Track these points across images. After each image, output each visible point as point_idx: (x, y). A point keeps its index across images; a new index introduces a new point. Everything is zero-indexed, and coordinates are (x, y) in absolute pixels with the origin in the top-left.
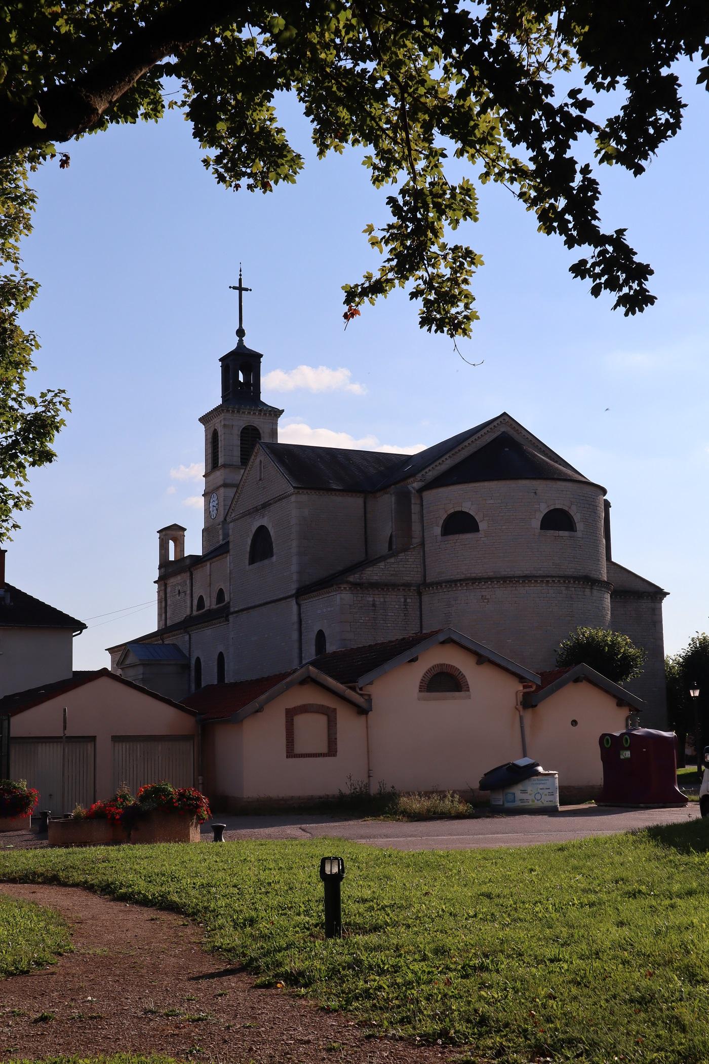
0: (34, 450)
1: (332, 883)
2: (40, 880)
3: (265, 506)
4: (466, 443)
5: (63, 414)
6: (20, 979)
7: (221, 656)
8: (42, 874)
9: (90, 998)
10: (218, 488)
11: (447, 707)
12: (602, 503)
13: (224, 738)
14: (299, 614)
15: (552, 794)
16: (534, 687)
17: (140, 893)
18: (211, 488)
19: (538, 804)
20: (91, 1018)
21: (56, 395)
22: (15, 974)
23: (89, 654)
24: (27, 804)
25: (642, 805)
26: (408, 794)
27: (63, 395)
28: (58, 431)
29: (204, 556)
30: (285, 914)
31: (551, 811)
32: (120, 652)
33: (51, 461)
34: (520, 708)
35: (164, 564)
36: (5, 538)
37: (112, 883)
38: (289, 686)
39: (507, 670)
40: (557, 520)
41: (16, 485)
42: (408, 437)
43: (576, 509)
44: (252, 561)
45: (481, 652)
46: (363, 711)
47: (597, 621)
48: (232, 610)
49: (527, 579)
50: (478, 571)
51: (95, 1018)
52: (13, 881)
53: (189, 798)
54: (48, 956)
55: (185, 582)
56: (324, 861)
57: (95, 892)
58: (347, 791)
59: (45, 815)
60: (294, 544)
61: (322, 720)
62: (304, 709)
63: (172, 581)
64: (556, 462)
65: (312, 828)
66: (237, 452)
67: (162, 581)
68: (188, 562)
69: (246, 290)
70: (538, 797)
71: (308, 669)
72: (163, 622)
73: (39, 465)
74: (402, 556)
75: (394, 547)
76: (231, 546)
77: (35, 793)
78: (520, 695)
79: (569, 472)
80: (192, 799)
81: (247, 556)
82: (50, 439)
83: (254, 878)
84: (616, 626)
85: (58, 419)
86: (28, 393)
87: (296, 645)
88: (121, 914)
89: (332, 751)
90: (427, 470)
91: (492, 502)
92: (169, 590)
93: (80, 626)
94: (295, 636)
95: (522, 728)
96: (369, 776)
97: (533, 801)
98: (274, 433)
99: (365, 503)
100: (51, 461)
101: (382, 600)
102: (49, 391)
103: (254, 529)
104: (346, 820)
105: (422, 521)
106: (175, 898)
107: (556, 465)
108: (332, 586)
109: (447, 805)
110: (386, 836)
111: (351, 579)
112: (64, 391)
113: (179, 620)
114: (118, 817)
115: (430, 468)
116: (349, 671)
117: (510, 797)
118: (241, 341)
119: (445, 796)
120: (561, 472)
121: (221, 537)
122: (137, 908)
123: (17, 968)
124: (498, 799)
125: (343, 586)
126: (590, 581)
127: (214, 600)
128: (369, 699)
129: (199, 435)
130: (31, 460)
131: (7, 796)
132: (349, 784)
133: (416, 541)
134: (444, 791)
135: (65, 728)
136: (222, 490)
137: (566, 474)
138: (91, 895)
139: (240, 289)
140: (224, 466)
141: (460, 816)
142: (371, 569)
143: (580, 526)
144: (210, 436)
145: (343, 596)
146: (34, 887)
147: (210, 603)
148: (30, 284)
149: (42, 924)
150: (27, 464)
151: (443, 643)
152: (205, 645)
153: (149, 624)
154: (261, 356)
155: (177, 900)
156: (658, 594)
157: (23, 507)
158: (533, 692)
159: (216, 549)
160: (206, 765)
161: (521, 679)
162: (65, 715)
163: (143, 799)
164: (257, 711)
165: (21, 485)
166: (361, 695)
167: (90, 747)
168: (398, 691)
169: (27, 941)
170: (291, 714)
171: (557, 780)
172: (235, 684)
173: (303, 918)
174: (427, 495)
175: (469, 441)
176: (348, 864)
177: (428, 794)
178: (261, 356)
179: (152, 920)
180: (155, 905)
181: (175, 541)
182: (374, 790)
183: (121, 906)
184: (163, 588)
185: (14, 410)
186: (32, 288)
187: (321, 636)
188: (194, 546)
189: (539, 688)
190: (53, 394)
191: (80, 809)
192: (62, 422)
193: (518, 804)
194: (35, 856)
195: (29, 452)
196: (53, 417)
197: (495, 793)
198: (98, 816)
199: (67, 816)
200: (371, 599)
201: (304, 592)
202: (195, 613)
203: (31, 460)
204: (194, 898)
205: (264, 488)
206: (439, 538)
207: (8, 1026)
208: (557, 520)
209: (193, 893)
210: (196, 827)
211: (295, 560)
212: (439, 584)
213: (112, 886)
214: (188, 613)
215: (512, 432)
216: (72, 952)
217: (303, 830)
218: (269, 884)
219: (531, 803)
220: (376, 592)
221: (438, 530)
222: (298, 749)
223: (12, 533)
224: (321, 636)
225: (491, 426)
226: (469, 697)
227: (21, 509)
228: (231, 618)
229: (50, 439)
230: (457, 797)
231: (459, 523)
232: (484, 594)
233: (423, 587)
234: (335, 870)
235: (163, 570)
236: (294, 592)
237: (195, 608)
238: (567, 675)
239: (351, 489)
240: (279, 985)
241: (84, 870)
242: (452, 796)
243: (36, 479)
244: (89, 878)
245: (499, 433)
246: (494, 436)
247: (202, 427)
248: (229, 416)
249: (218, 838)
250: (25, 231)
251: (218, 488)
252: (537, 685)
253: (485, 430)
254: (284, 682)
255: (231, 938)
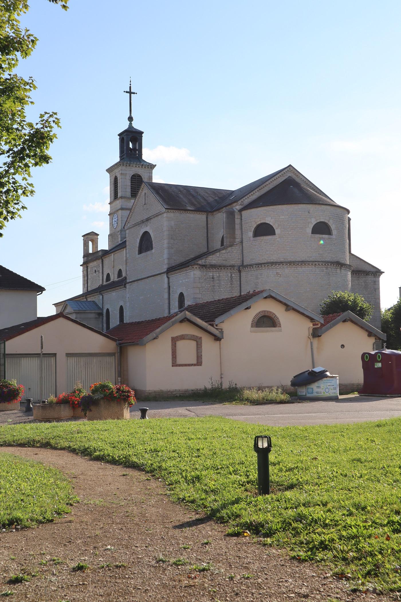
0: (35, 155)
1: (263, 455)
2: (38, 445)
3: (148, 220)
4: (267, 183)
5: (55, 130)
6: (48, 526)
7: (121, 308)
8: (39, 441)
9: (109, 547)
10: (118, 210)
11: (267, 335)
12: (347, 219)
13: (134, 355)
14: (169, 283)
15: (335, 389)
16: (319, 325)
17: (109, 455)
18: (114, 210)
19: (327, 395)
20: (117, 567)
21: (51, 116)
22: (43, 523)
23: (45, 307)
24: (18, 394)
25: (388, 395)
26: (250, 388)
27: (55, 116)
28: (52, 142)
29: (110, 250)
30: (219, 473)
31: (335, 399)
32: (62, 305)
33: (48, 163)
34: (311, 337)
35: (86, 255)
36: (16, 216)
37: (88, 448)
38: (173, 324)
39: (303, 314)
40: (321, 229)
41: (23, 180)
42: (232, 178)
43: (331, 223)
44: (140, 252)
45: (289, 303)
46: (217, 339)
47: (344, 288)
48: (128, 281)
49: (303, 263)
50: (274, 258)
51: (120, 567)
52: (22, 445)
53: (123, 392)
54: (63, 507)
55: (99, 265)
56: (257, 438)
57: (77, 454)
58: (209, 386)
59: (29, 401)
60: (166, 242)
61: (193, 344)
62: (182, 337)
63: (91, 265)
64: (318, 193)
65: (193, 409)
66: (129, 190)
67: (85, 264)
68: (100, 254)
69: (134, 93)
70: (327, 390)
71: (185, 313)
72: (86, 289)
73: (40, 166)
74: (229, 249)
75: (225, 244)
76: (127, 243)
77: (22, 388)
78: (311, 330)
79: (328, 200)
80: (125, 392)
81: (137, 249)
82: (47, 147)
83: (185, 446)
84: (353, 290)
85: (51, 134)
86: (28, 120)
87: (167, 301)
88: (100, 471)
89: (199, 363)
90: (244, 198)
91: (283, 217)
92: (89, 270)
93: (41, 289)
94: (166, 296)
95: (312, 349)
96: (221, 378)
97: (324, 393)
98: (151, 178)
99: (207, 218)
100: (48, 163)
101: (218, 275)
102: (46, 113)
103: (141, 233)
104: (212, 404)
105: (242, 229)
106: (135, 459)
107: (321, 196)
108: (189, 266)
109: (273, 395)
110: (242, 415)
111: (200, 262)
112: (56, 114)
113: (95, 288)
114: (77, 402)
115: (246, 197)
116: (210, 314)
117: (310, 390)
118: (131, 124)
119: (272, 390)
120: (321, 199)
121: (120, 239)
122: (109, 466)
123: (44, 518)
124: (302, 391)
125: (195, 266)
126: (340, 265)
127: (116, 276)
128: (222, 332)
129: (107, 179)
130: (33, 162)
131: (5, 390)
132: (211, 382)
133: (238, 240)
134: (271, 387)
135: (42, 348)
136: (120, 212)
137: (326, 201)
138: (75, 456)
139: (130, 93)
140: (121, 197)
141: (282, 402)
142: (211, 256)
143: (334, 232)
144: (113, 180)
145: (195, 272)
146: (36, 450)
147: (114, 278)
148: (32, 38)
149: (52, 480)
150: (30, 165)
151: (266, 298)
152: (112, 301)
153: (78, 290)
154: (143, 133)
155: (136, 460)
156: (377, 273)
157: (29, 194)
158: (318, 328)
159: (118, 246)
160: (122, 372)
161: (312, 320)
162: (42, 340)
163: (94, 392)
164: (155, 339)
165: (26, 180)
166: (217, 329)
167: (53, 359)
168: (238, 325)
169: (45, 494)
170: (174, 340)
171: (338, 380)
172: (131, 324)
173: (233, 477)
174: (244, 213)
175: (269, 181)
176: (273, 440)
177: (260, 389)
178: (143, 133)
179: (124, 475)
180: (121, 464)
181: (92, 241)
182: (226, 386)
183: (96, 465)
184: (86, 269)
185: (19, 130)
186: (33, 41)
187: (181, 295)
188: (103, 244)
189: (322, 325)
190: (48, 115)
191: (52, 398)
192: (55, 136)
193: (315, 395)
194: (32, 429)
195: (33, 156)
196: (49, 131)
197: (302, 387)
198: (64, 402)
199: (44, 402)
200: (211, 274)
201: (171, 270)
202: (105, 283)
203: (33, 162)
204: (147, 460)
205: (147, 209)
206: (252, 238)
207: (53, 574)
208: (321, 229)
209: (146, 456)
210: (127, 409)
211: (166, 251)
212: (251, 266)
213: (89, 450)
214: (101, 283)
215: (294, 177)
216: (78, 502)
217: (189, 411)
218: (198, 450)
219: (323, 394)
220: (215, 270)
221: (251, 234)
222: (179, 362)
223: (21, 212)
224: (181, 295)
225: (282, 173)
226: (281, 331)
227: (27, 196)
228: (127, 286)
229: (47, 147)
230: (280, 390)
231: (264, 230)
232: (278, 271)
233: (241, 267)
234: (266, 445)
235: (86, 258)
236: (165, 270)
237: (105, 280)
238: (339, 318)
239: (199, 210)
240: (245, 534)
241: (66, 439)
242: (277, 390)
243: (37, 175)
244: (71, 444)
245: (287, 177)
246: (285, 178)
247: (108, 175)
248: (124, 168)
249: (143, 416)
250: (24, 10)
251: (118, 210)
252: (321, 324)
253: (278, 175)
254: (171, 321)
255: (188, 492)
